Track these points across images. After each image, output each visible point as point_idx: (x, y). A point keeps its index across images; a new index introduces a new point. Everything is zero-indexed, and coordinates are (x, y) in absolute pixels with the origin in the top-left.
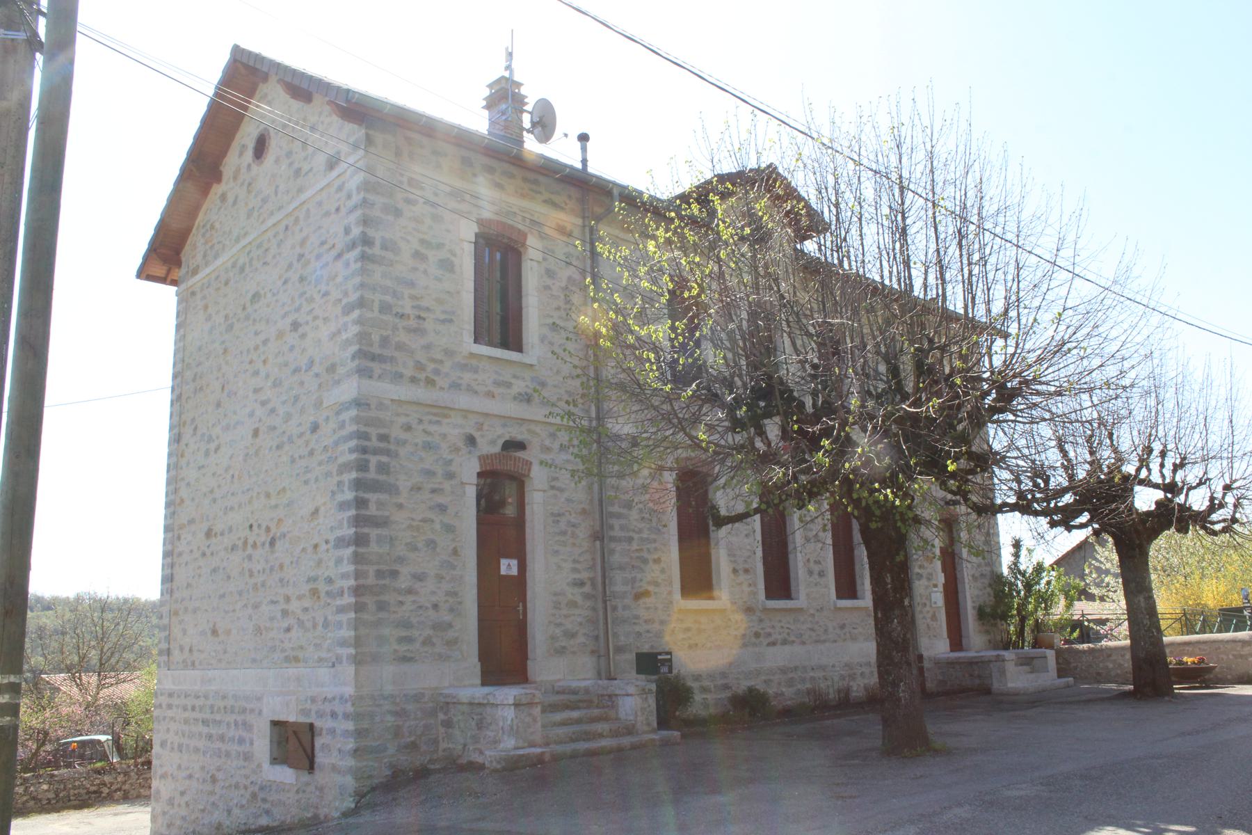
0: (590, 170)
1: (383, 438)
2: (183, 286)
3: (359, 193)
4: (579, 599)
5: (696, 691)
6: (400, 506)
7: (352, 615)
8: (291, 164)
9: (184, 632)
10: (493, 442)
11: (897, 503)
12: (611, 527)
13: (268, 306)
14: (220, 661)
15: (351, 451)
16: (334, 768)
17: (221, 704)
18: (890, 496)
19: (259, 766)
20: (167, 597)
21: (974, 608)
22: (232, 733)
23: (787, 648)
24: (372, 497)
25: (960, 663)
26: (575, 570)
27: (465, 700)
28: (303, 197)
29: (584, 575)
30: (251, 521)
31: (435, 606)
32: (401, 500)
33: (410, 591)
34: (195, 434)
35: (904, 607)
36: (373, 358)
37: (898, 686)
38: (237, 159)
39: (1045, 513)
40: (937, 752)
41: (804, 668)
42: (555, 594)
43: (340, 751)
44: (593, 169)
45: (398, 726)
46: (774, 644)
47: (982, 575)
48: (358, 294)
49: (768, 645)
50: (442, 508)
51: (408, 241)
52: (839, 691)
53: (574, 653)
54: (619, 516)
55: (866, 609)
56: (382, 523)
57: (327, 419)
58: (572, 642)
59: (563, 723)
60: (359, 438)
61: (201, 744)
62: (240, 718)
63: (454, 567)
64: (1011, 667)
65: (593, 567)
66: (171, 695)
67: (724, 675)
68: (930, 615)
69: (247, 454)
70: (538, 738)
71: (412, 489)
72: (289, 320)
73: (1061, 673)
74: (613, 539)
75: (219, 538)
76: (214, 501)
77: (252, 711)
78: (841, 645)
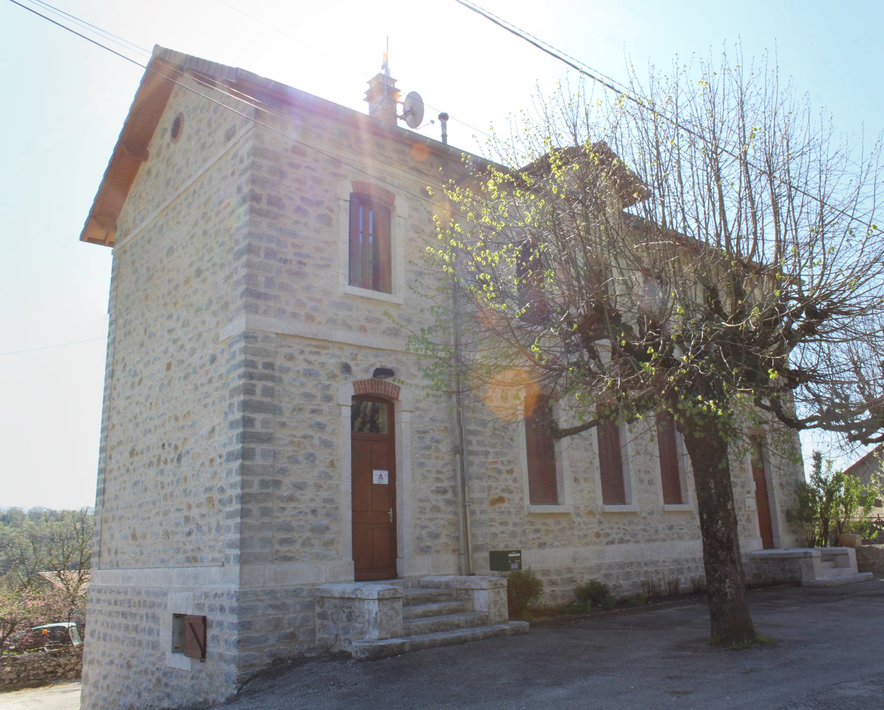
0: (449, 143)
1: (269, 366)
2: (118, 246)
3: (249, 157)
4: (442, 505)
5: (545, 585)
6: (283, 425)
7: (238, 520)
8: (199, 140)
9: (112, 536)
10: (366, 370)
11: (720, 413)
12: (470, 443)
13: (179, 257)
14: (137, 561)
15: (240, 377)
16: (221, 657)
17: (136, 599)
18: (713, 406)
19: (163, 654)
20: (100, 507)
21: (783, 511)
22: (144, 624)
23: (624, 547)
24: (258, 417)
25: (773, 559)
26: (438, 480)
27: (337, 595)
28: (207, 165)
29: (446, 484)
30: (164, 441)
31: (314, 512)
32: (284, 420)
33: (291, 499)
34: (124, 370)
35: (728, 510)
36: (259, 296)
37: (724, 582)
38: (160, 140)
39: (846, 429)
40: (762, 644)
41: (639, 563)
42: (421, 501)
43: (226, 642)
44: (450, 142)
45: (279, 619)
46: (612, 543)
47: (788, 483)
48: (246, 242)
49: (607, 543)
50: (321, 427)
51: (291, 198)
52: (669, 584)
53: (438, 552)
54: (476, 433)
55: (690, 512)
56: (268, 439)
57: (223, 350)
58: (436, 542)
59: (425, 615)
60: (246, 366)
61: (121, 634)
62: (150, 611)
63: (330, 477)
64: (817, 563)
65: (454, 477)
66: (99, 591)
67: (569, 570)
68: (745, 517)
69: (162, 385)
70: (399, 629)
71: (294, 410)
72: (194, 268)
73: (861, 568)
74: (472, 453)
75: (140, 456)
76: (137, 425)
77: (160, 605)
78: (675, 547)
